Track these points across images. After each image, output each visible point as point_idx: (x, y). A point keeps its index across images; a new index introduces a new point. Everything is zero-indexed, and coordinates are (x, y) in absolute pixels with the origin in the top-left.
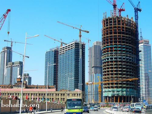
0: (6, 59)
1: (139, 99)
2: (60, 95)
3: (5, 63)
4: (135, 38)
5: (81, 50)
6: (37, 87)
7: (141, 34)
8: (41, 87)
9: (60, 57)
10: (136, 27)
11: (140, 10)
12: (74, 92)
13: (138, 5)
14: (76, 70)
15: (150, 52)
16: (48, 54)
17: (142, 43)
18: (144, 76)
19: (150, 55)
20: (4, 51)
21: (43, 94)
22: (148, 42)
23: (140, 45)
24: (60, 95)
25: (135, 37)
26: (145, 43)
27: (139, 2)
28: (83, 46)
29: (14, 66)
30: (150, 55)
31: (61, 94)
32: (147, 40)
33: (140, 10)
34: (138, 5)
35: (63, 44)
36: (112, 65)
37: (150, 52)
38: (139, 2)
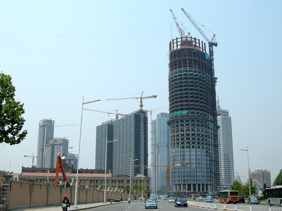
0: (46, 134)
1: (218, 187)
2: (117, 182)
3: (45, 142)
4: (209, 64)
5: (142, 124)
6: (87, 171)
7: (219, 103)
8: (92, 171)
9: (116, 132)
10: (211, 61)
11: (216, 45)
12: (136, 178)
13: (213, 39)
14: (136, 126)
15: (232, 157)
16: (99, 129)
17: (220, 115)
18: (223, 162)
19: (230, 136)
20: (43, 125)
21: (96, 181)
22: (228, 113)
23: (218, 117)
24: (117, 182)
25: (212, 96)
26: (224, 115)
27: (215, 35)
28: (146, 119)
29: (56, 145)
30: (230, 136)
31: (119, 181)
32: (227, 112)
33: (216, 45)
34: (213, 39)
35: (119, 116)
36: (181, 83)
37: (232, 157)
38: (215, 35)
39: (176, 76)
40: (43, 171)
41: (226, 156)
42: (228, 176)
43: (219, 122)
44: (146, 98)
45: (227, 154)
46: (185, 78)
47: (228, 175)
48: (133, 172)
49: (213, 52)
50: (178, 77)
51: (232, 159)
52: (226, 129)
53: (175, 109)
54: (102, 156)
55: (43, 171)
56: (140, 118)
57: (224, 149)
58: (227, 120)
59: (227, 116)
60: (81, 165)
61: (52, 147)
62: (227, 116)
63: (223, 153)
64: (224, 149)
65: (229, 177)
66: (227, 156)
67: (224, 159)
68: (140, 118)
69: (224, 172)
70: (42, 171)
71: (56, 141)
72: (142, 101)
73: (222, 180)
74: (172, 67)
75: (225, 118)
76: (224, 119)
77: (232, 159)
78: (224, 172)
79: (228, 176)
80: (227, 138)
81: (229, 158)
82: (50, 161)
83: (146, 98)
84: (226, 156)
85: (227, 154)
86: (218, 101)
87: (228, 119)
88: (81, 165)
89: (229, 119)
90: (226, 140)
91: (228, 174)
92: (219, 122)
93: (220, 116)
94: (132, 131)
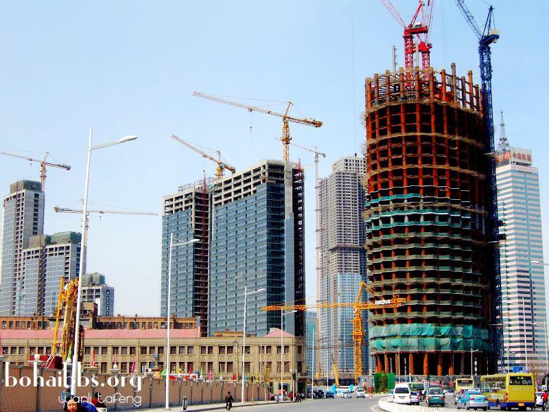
2: (216, 350)
8: (149, 323)
11: (543, 410)
17: (506, 162)
20: (15, 197)
23: (499, 170)
24: (216, 350)
26: (517, 163)
30: (537, 226)
31: (221, 348)
39: (386, 220)
40: (14, 325)
41: (524, 277)
42: (529, 290)
43: (500, 179)
44: (299, 121)
45: (526, 272)
46: (411, 229)
47: (528, 287)
48: (264, 322)
49: (490, 67)
50: (393, 224)
51: (540, 249)
52: (531, 238)
53: (383, 252)
54: (180, 293)
55: (14, 325)
56: (279, 184)
57: (514, 180)
58: (528, 176)
59: (527, 165)
60: (122, 308)
61: (40, 261)
62: (527, 165)
63: (515, 268)
64: (514, 180)
65: (531, 293)
66: (528, 277)
67: (518, 276)
68: (279, 184)
69: (516, 290)
70: (11, 323)
71: (49, 240)
72: (287, 127)
73: (512, 344)
74: (373, 127)
75: (520, 172)
76: (518, 175)
77: (540, 249)
78: (516, 290)
79: (529, 290)
80: (525, 227)
81: (531, 282)
82: (37, 278)
83: (299, 121)
84: (524, 277)
85: (526, 272)
86: (502, 125)
87: (530, 173)
88: (122, 308)
89: (534, 177)
90: (522, 211)
91: (529, 285)
92: (500, 179)
93: (508, 167)
94: (261, 218)
